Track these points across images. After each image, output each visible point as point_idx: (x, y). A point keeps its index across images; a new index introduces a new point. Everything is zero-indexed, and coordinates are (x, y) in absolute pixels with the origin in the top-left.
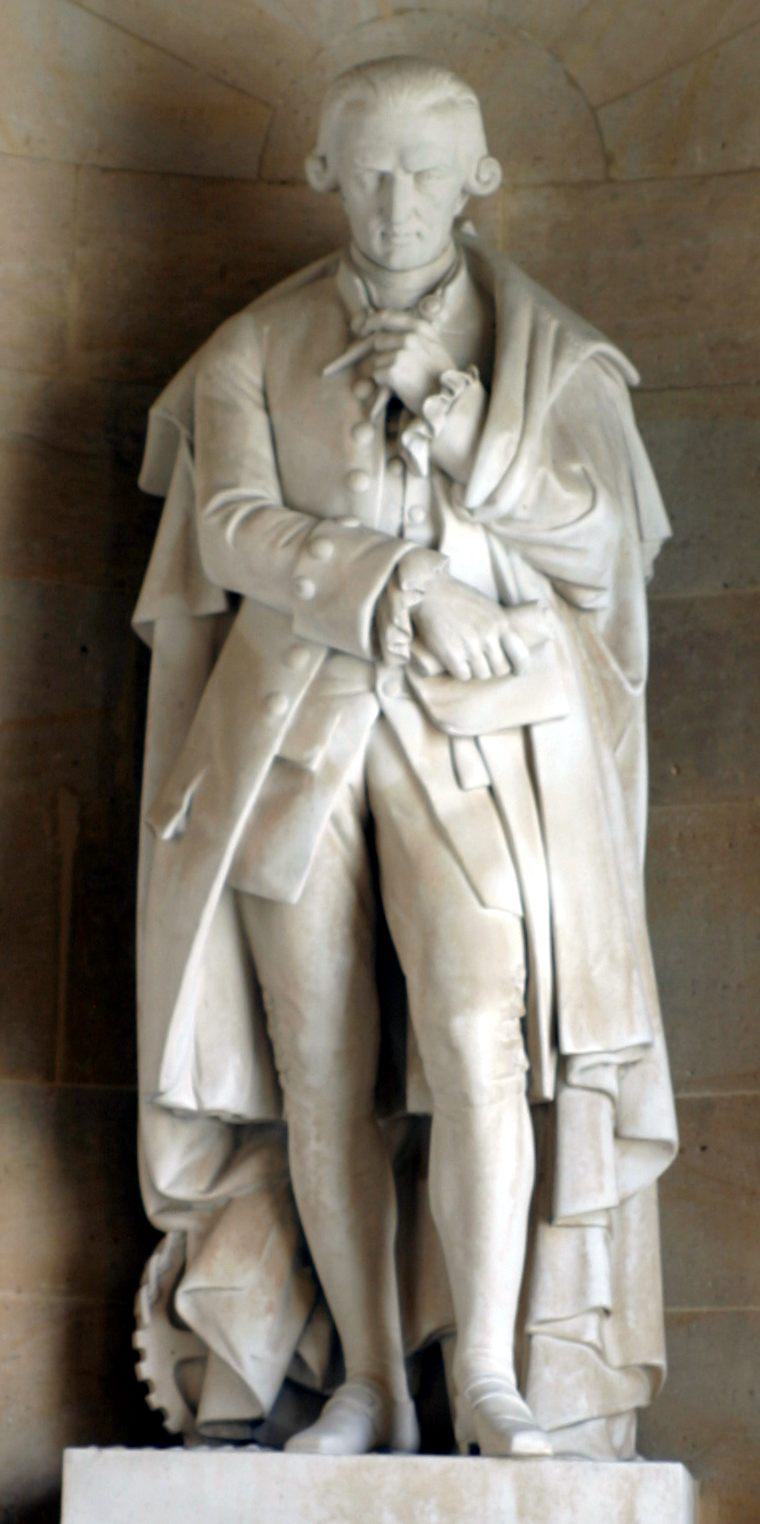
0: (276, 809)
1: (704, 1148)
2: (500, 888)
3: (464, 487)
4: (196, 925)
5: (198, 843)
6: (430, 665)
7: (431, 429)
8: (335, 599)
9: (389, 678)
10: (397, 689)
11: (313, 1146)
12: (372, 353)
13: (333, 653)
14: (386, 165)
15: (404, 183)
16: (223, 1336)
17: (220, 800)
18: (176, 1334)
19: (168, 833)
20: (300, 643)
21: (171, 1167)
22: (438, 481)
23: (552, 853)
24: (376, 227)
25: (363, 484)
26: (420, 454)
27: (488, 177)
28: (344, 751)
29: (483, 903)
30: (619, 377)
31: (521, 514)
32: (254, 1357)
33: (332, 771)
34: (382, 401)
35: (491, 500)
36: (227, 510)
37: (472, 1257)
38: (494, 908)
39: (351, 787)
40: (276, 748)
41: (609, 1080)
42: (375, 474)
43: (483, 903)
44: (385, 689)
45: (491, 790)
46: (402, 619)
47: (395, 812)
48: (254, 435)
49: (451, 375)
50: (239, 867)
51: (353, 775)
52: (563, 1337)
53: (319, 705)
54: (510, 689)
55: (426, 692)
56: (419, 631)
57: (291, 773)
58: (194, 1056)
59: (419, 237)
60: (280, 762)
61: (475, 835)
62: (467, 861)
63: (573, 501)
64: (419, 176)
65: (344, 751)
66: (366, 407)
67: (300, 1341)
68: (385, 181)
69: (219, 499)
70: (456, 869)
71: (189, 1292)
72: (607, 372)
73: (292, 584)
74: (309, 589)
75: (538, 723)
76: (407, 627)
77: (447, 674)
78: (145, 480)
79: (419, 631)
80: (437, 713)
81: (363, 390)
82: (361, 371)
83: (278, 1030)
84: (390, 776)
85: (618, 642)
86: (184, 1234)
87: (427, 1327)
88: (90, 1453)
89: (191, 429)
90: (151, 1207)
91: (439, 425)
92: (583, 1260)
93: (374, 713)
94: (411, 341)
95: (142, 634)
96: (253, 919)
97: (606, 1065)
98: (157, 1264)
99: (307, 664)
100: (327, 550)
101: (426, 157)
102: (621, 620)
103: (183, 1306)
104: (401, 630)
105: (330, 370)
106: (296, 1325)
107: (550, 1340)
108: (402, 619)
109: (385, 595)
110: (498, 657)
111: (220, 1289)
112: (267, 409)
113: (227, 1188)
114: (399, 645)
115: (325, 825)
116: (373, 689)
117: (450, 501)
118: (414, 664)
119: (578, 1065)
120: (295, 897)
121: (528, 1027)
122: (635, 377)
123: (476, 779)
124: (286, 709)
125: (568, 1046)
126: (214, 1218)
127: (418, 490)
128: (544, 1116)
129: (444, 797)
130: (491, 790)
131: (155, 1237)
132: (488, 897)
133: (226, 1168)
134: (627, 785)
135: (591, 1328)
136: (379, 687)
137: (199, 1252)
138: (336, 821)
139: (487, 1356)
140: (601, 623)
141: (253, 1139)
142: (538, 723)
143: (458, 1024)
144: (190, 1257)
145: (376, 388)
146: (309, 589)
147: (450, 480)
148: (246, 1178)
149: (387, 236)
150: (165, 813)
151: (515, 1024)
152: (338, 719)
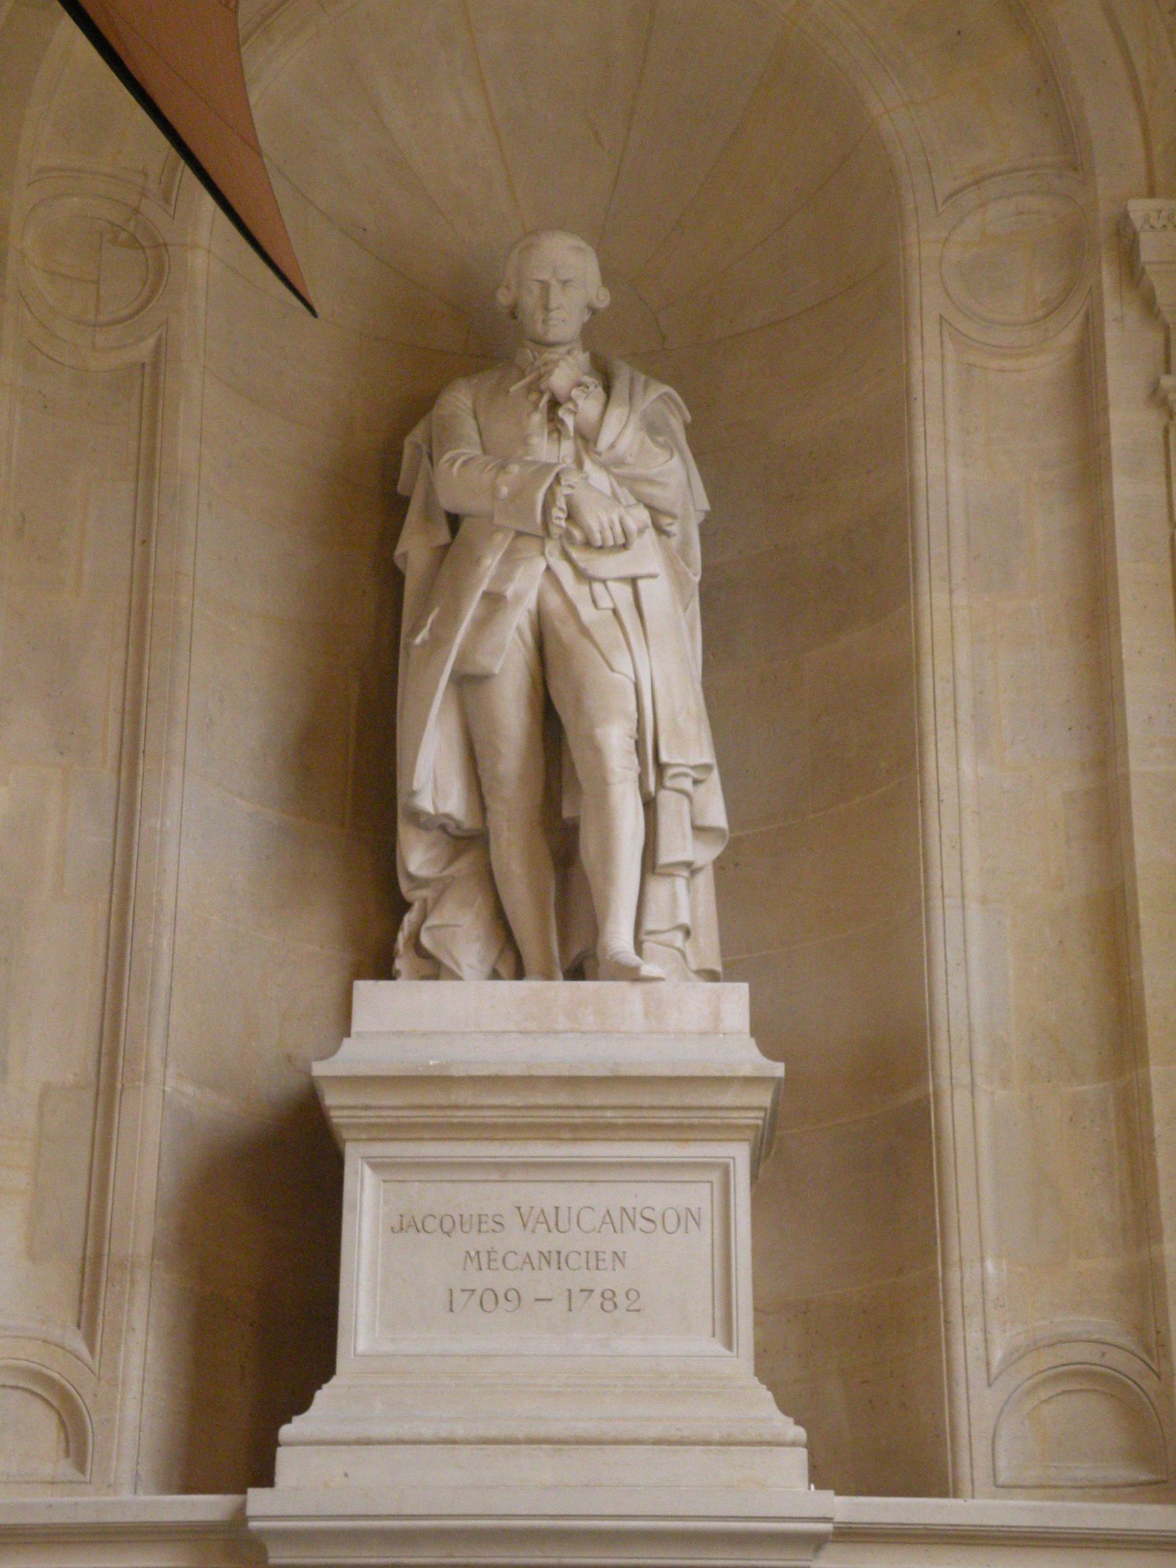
0: (483, 623)
1: (736, 865)
2: (623, 663)
3: (595, 442)
4: (436, 687)
5: (438, 642)
6: (577, 534)
7: (576, 405)
8: (521, 493)
9: (551, 547)
10: (557, 553)
11: (506, 834)
12: (541, 376)
13: (519, 534)
14: (545, 276)
15: (555, 288)
16: (450, 954)
17: (451, 617)
18: (423, 962)
19: (418, 640)
20: (499, 528)
21: (417, 857)
22: (579, 442)
23: (652, 650)
24: (539, 316)
25: (535, 440)
26: (569, 421)
27: (602, 298)
28: (526, 586)
29: (612, 670)
30: (678, 415)
31: (630, 460)
32: (469, 966)
33: (518, 597)
34: (546, 398)
35: (612, 446)
36: (454, 460)
37: (608, 878)
38: (619, 672)
39: (529, 611)
40: (484, 586)
41: (687, 784)
42: (542, 436)
43: (612, 670)
44: (550, 553)
45: (615, 612)
46: (561, 502)
47: (557, 624)
48: (469, 427)
49: (587, 379)
50: (462, 658)
51: (530, 602)
52: (660, 944)
53: (510, 560)
54: (624, 556)
55: (575, 554)
56: (571, 517)
57: (494, 600)
58: (433, 776)
59: (565, 319)
60: (487, 595)
61: (606, 633)
62: (602, 647)
63: (661, 455)
64: (565, 283)
65: (526, 586)
66: (536, 406)
67: (496, 964)
68: (545, 286)
69: (446, 457)
70: (596, 652)
71: (429, 928)
72: (672, 413)
73: (494, 490)
74: (505, 491)
75: (641, 577)
76: (564, 507)
77: (588, 544)
78: (401, 488)
79: (571, 517)
80: (582, 565)
81: (534, 396)
82: (536, 387)
83: (483, 764)
84: (554, 602)
85: (685, 543)
86: (425, 901)
87: (575, 950)
88: (370, 983)
89: (430, 447)
90: (404, 886)
91: (580, 402)
92: (674, 897)
93: (543, 567)
94: (562, 364)
95: (400, 565)
96: (470, 684)
97: (686, 775)
98: (409, 918)
99: (502, 542)
100: (515, 469)
101: (567, 279)
102: (685, 543)
103: (425, 940)
104: (561, 509)
105: (513, 389)
106: (493, 955)
107: (654, 945)
108: (561, 502)
109: (551, 487)
110: (618, 529)
111: (448, 926)
112: (476, 417)
113: (451, 870)
114: (558, 518)
115: (511, 636)
116: (543, 554)
117: (587, 451)
118: (568, 535)
119: (671, 772)
120: (497, 670)
121: (639, 745)
122: (689, 418)
123: (605, 602)
124: (491, 563)
125: (664, 757)
126: (442, 887)
127: (567, 447)
128: (650, 805)
129: (587, 613)
130: (615, 612)
131: (406, 906)
132: (615, 667)
133: (451, 861)
134: (692, 636)
135: (678, 938)
136: (546, 551)
137: (432, 910)
138: (519, 630)
139: (619, 937)
140: (674, 542)
141: (468, 842)
142: (641, 577)
143: (599, 732)
144: (429, 908)
145: (542, 393)
146: (505, 491)
147: (587, 439)
148: (463, 865)
149: (545, 321)
150: (415, 630)
151: (632, 742)
152: (522, 567)
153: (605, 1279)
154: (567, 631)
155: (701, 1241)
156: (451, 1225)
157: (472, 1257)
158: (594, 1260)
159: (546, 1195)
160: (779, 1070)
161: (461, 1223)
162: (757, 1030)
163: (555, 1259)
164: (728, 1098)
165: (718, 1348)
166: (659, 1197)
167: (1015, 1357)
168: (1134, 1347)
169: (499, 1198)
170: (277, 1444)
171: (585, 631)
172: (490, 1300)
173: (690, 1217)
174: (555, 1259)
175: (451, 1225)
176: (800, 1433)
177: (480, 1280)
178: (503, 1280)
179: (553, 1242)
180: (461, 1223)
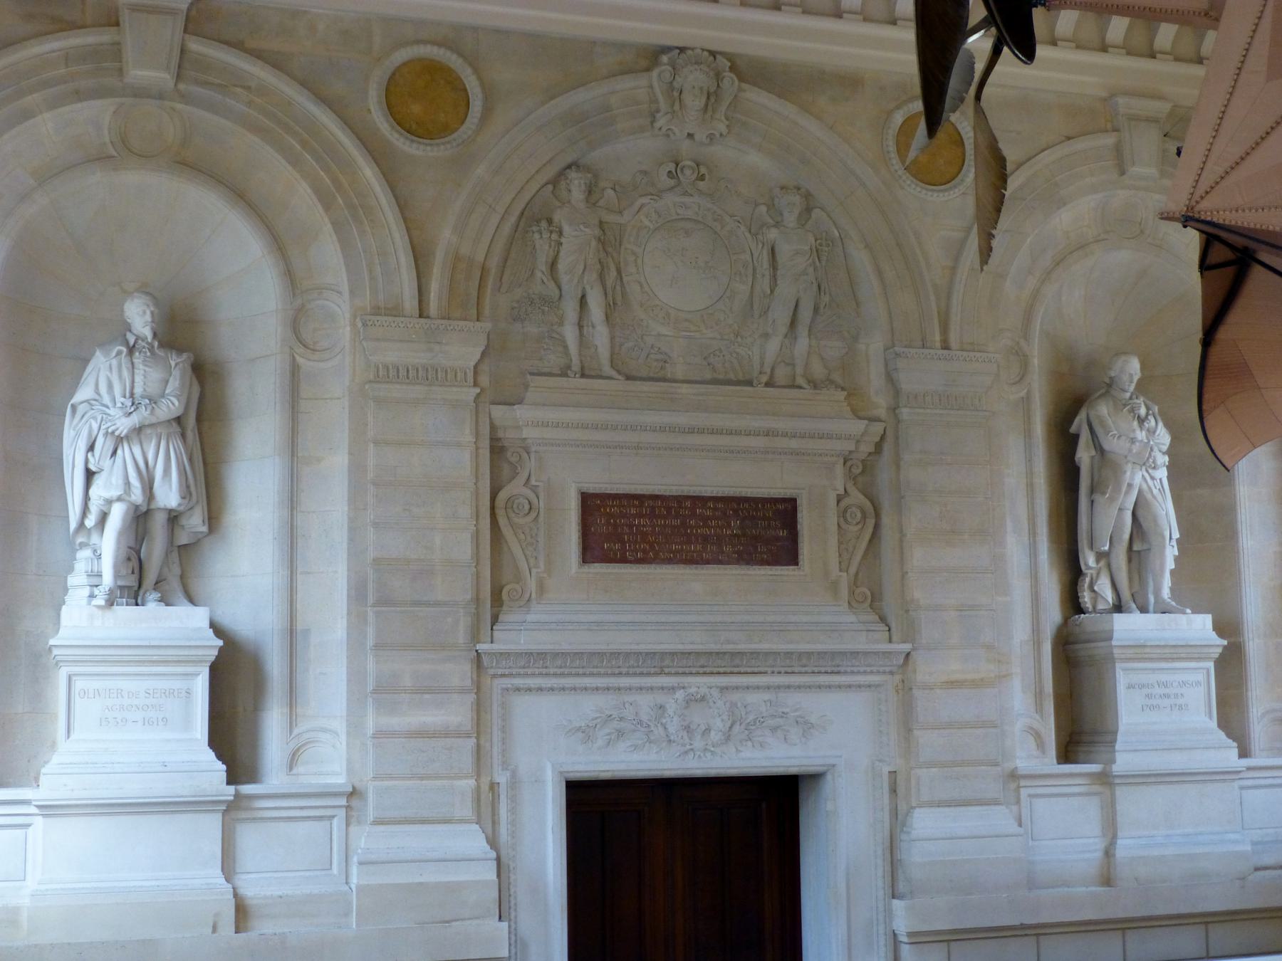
53: (1133, 474)
73: (1130, 450)
84: (1145, 487)
153: (1180, 701)
154: (1149, 496)
155: (1202, 690)
156: (1142, 686)
157: (1147, 696)
158: (1176, 696)
159: (1164, 677)
160: (1225, 643)
161: (1143, 686)
162: (1215, 629)
163: (1167, 696)
164: (1211, 650)
165: (1207, 719)
166: (1191, 677)
167: (1263, 715)
168: (1015, 549)
169: (1152, 678)
170: (66, 590)
171: (1154, 497)
172: (1152, 708)
173: (1198, 683)
174: (1167, 696)
175: (1142, 686)
176: (1235, 744)
177: (1150, 702)
178: (1155, 702)
179: (1167, 691)
180: (1143, 686)
